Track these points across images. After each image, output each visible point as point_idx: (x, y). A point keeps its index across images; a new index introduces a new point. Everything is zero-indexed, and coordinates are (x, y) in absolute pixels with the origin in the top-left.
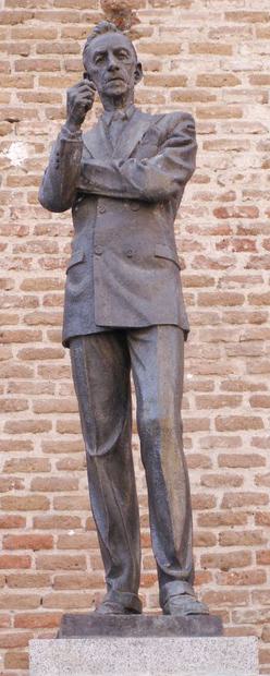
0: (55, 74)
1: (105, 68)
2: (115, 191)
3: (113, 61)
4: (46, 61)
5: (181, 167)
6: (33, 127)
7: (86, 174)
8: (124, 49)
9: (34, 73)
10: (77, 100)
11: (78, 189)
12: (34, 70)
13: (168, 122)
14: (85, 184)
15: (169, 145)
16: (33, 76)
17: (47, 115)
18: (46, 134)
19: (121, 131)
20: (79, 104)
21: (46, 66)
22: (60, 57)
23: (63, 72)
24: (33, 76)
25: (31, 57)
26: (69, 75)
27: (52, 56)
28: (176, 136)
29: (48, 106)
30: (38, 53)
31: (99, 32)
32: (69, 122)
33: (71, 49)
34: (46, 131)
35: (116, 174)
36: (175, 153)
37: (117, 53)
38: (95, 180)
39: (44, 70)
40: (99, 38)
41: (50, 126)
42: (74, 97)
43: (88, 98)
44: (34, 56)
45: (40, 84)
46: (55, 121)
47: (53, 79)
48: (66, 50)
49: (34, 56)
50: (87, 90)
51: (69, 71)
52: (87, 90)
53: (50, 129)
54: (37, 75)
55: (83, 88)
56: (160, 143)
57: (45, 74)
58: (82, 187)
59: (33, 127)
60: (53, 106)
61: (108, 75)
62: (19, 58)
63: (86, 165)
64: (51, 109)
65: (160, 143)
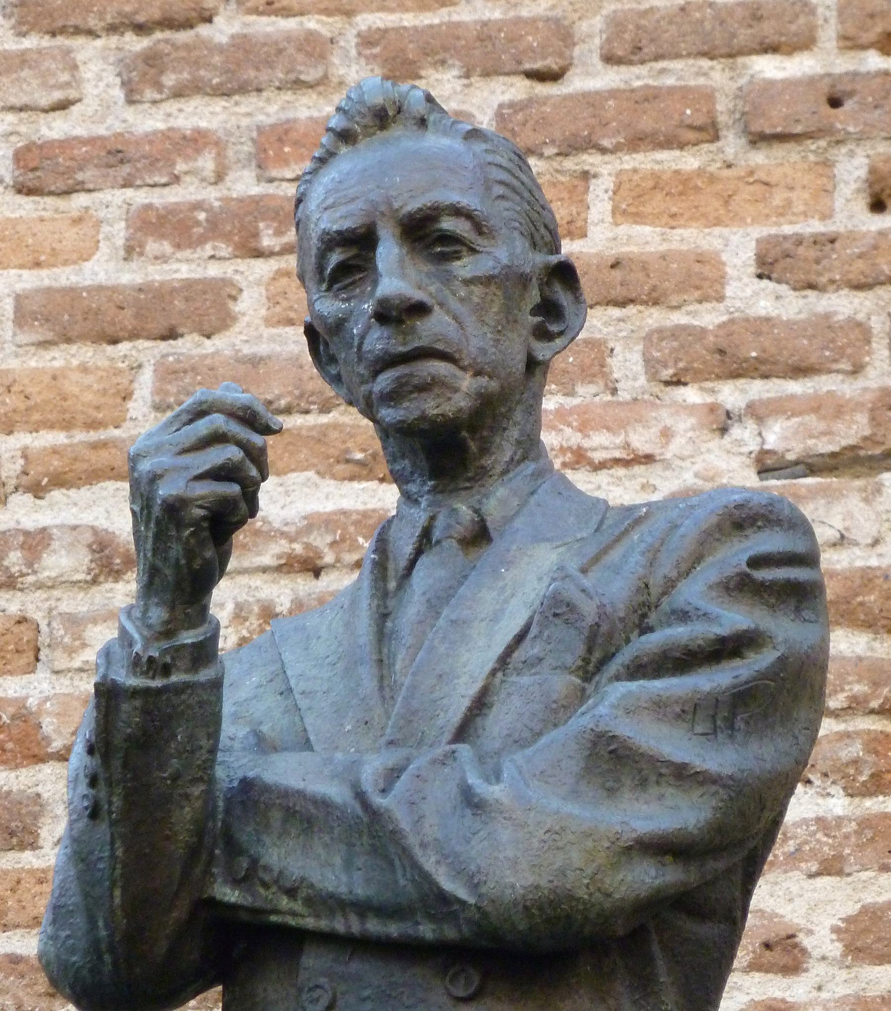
0: (688, 161)
1: (368, 307)
2: (363, 908)
3: (395, 274)
4: (651, 96)
5: (683, 775)
6: (583, 428)
7: (245, 834)
8: (457, 211)
9: (590, 160)
10: (165, 490)
11: (213, 903)
12: (591, 145)
13: (653, 556)
14: (237, 883)
15: (639, 670)
16: (586, 176)
17: (651, 365)
18: (648, 459)
19: (437, 603)
20: (174, 509)
21: (646, 123)
22: (716, 76)
23: (732, 144)
24: (586, 176)
25: (576, 83)
26: (759, 158)
27: (678, 73)
28: (683, 616)
29: (655, 318)
30: (610, 59)
31: (346, 136)
32: (151, 586)
33: (768, 30)
34: (641, 440)
35: (371, 831)
36: (659, 706)
37: (423, 232)
38: (287, 857)
39: (638, 142)
40: (348, 163)
41: (666, 417)
42: (155, 478)
43: (220, 474)
44: (591, 78)
45: (620, 214)
46: (691, 394)
47: (685, 184)
48: (744, 35)
49: (591, 78)
50: (217, 438)
51: (759, 139)
52: (217, 438)
53: (667, 434)
54: (606, 169)
55: (203, 427)
56: (591, 668)
57: (646, 161)
58: (230, 895)
59: (583, 428)
60: (679, 318)
61: (378, 341)
62: (518, 89)
63: (247, 785)
64: (676, 332)
65: (591, 668)
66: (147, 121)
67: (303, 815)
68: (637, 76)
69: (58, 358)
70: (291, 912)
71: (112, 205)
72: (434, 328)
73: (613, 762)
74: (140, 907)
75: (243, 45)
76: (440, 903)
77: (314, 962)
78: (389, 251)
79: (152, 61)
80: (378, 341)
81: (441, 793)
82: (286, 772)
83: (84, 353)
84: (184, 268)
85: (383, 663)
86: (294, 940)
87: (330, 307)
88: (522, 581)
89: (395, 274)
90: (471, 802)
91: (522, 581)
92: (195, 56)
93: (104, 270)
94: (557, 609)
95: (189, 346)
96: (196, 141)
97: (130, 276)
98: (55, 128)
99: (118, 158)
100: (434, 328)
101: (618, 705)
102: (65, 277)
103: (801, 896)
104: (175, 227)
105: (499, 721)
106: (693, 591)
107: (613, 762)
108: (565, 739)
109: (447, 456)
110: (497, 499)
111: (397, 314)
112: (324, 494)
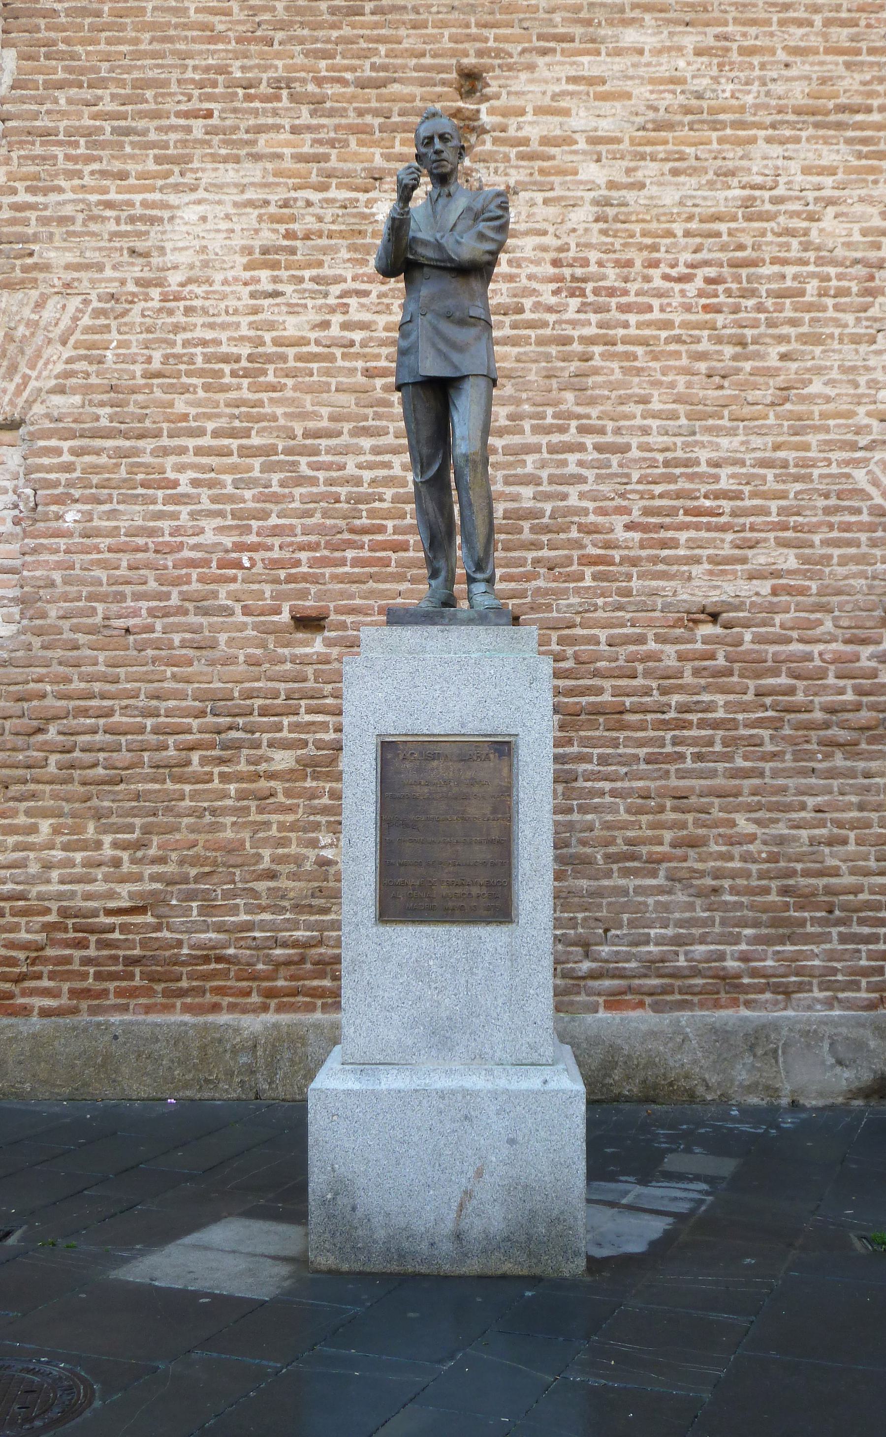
3: (438, 145)
5: (493, 240)
19: (445, 206)
20: (406, 186)
25: (393, 119)
35: (439, 247)
37: (443, 137)
38: (421, 250)
54: (399, 136)
56: (476, 218)
61: (434, 157)
66: (314, 122)
67: (425, 243)
68: (404, 119)
69: (299, 166)
70: (422, 260)
71: (308, 137)
72: (444, 155)
73: (482, 236)
74: (396, 257)
75: (332, 108)
76: (451, 260)
77: (426, 269)
78: (437, 140)
79: (315, 110)
80: (434, 157)
81: (451, 241)
82: (420, 235)
83: (303, 165)
84: (321, 150)
85: (435, 217)
86: (421, 266)
87: (423, 150)
88: (460, 203)
89: (438, 145)
90: (458, 242)
91: (460, 203)
92: (323, 109)
93: (306, 149)
94: (469, 209)
95: (322, 165)
96: (323, 126)
97: (312, 151)
98: (297, 122)
99: (309, 128)
100: (444, 155)
101: (482, 226)
102: (299, 150)
103: (276, 294)
104: (320, 142)
105: (459, 228)
106: (492, 206)
107: (482, 236)
108: (474, 231)
109: (442, 179)
110: (452, 188)
111: (438, 152)
112: (425, 186)
